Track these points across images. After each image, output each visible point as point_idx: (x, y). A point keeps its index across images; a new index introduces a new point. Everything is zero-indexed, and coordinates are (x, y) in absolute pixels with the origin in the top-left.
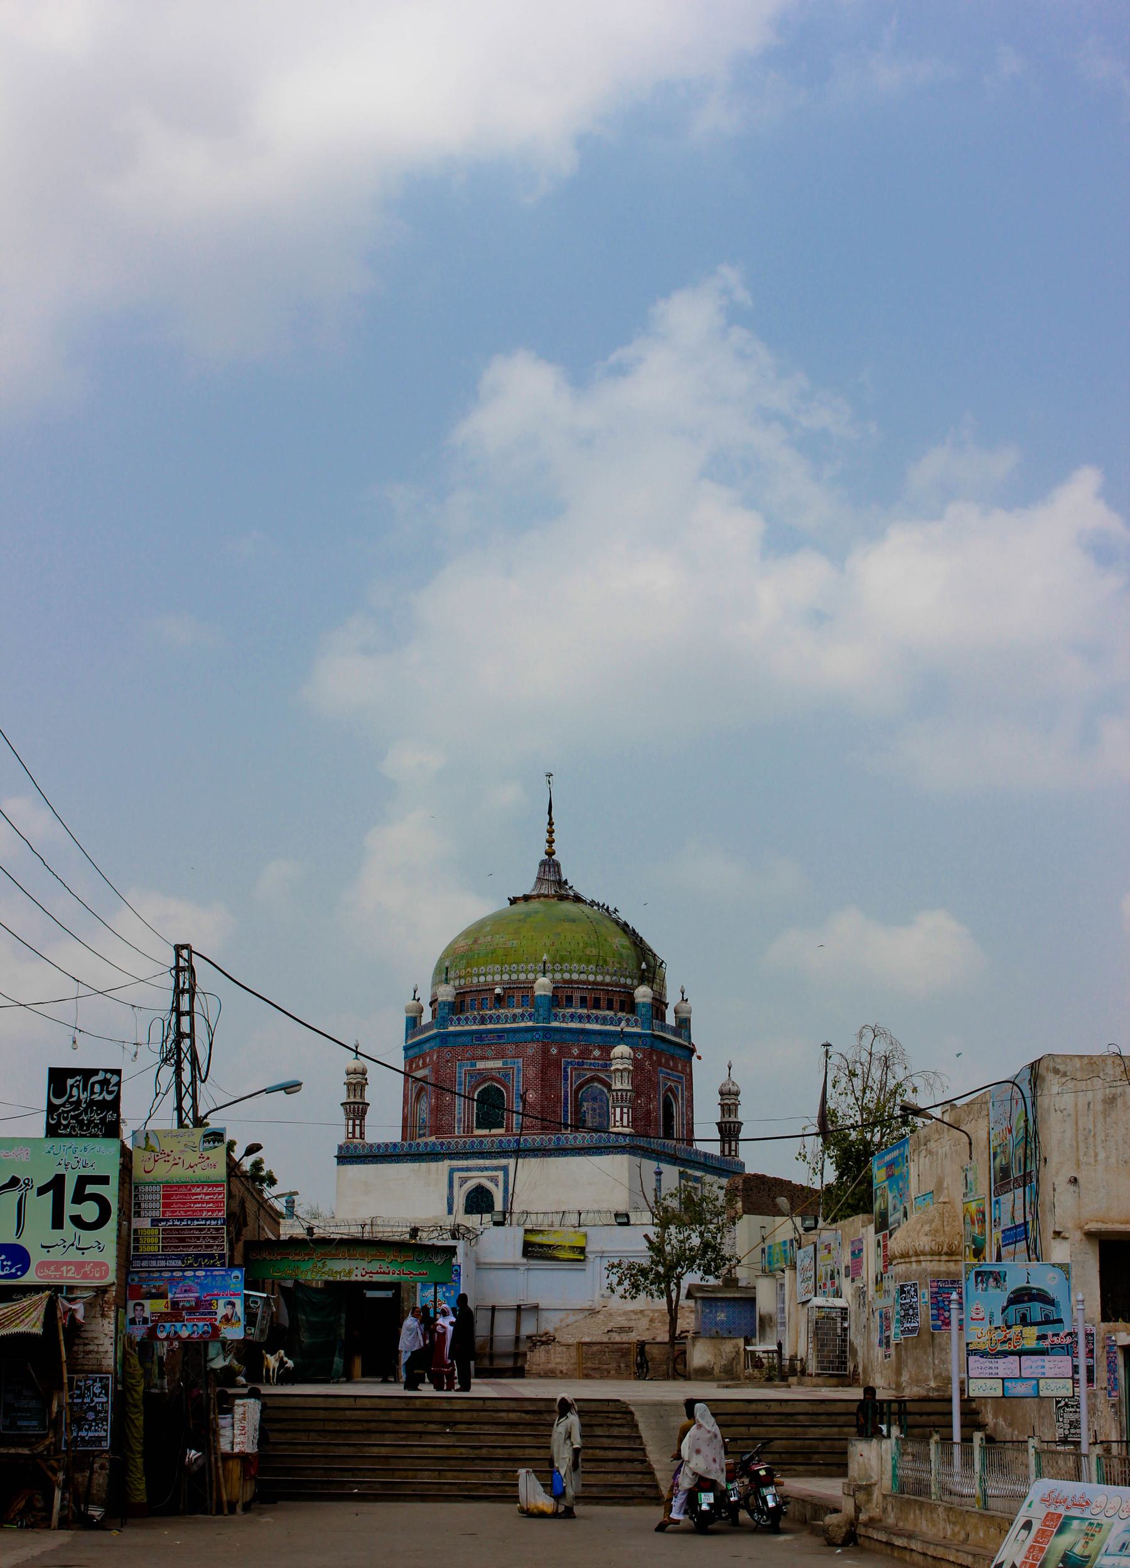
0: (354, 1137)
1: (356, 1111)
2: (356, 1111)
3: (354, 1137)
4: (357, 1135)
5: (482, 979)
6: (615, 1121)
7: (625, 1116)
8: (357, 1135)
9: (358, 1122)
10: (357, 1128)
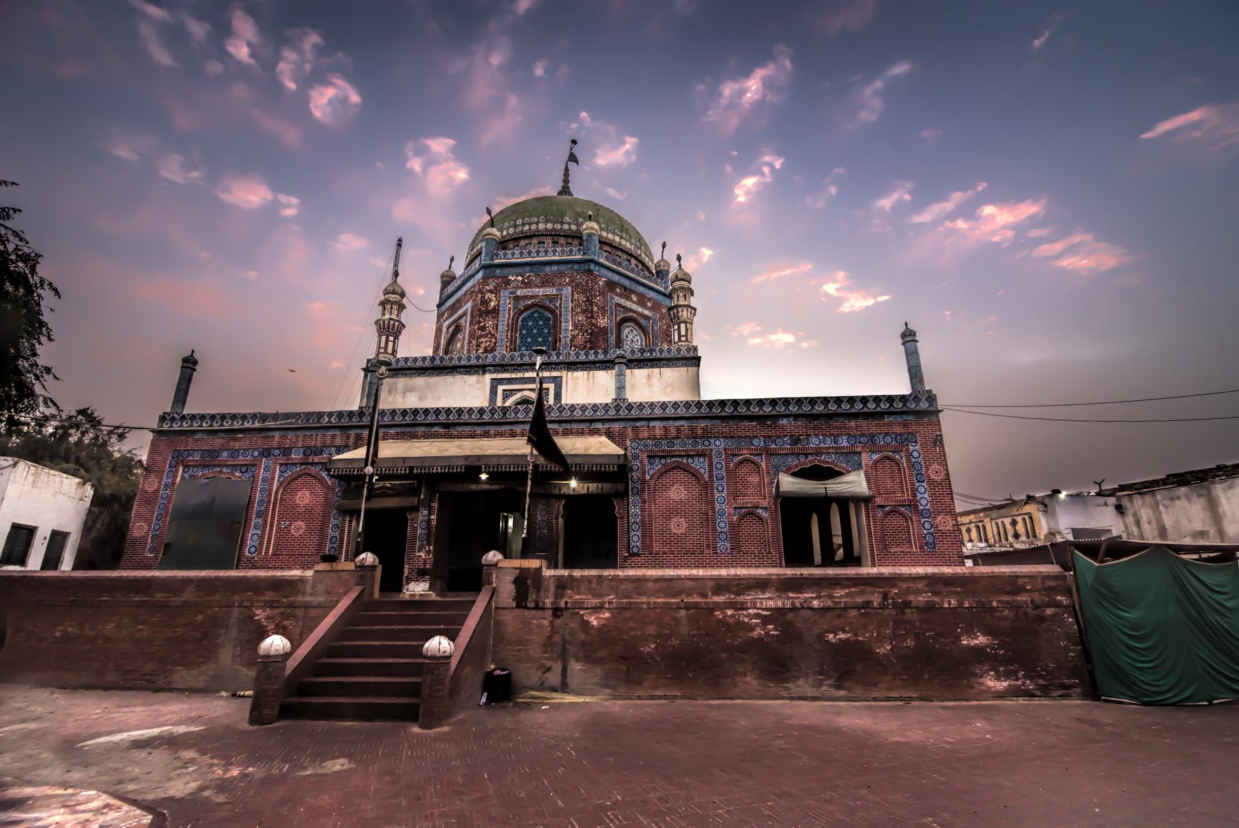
1: (390, 330)
2: (390, 330)
3: (386, 352)
4: (390, 350)
5: (527, 228)
6: (680, 336)
7: (683, 333)
8: (390, 350)
9: (391, 338)
10: (390, 344)
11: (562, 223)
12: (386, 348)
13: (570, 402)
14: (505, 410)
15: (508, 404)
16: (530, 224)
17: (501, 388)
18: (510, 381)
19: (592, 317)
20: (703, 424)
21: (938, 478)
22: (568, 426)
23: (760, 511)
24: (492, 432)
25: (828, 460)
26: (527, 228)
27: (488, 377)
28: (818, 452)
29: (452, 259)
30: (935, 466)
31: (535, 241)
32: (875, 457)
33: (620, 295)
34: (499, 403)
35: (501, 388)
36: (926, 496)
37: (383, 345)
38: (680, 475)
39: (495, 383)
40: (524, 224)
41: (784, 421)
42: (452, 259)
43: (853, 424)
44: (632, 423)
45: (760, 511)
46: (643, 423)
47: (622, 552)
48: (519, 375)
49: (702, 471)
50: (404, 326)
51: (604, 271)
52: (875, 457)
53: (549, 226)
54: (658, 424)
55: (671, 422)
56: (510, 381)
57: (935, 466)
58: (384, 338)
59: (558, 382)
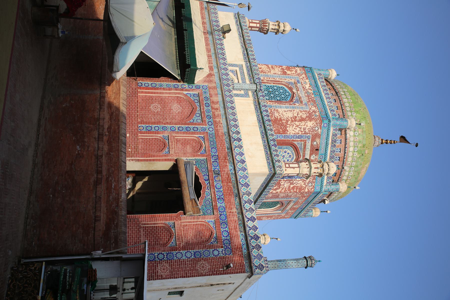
0: (250, 22)
5: (342, 93)
7: (291, 165)
8: (252, 25)
9: (258, 25)
10: (255, 25)
11: (351, 111)
12: (252, 23)
13: (236, 101)
14: (227, 75)
15: (231, 74)
16: (345, 94)
17: (238, 69)
18: (242, 73)
19: (292, 121)
20: (223, 121)
21: (198, 267)
22: (213, 57)
23: (167, 150)
24: (205, 25)
25: (206, 192)
26: (342, 93)
27: (244, 63)
28: (212, 186)
29: (319, 261)
30: (208, 266)
31: (336, 97)
32: (212, 225)
33: (312, 145)
34: (230, 68)
35: (238, 69)
36: (184, 258)
37: (253, 21)
38: (187, 111)
39: (241, 67)
40: (344, 92)
41: (230, 167)
42: (319, 261)
43: (234, 210)
44: (219, 86)
45: (167, 150)
46: (220, 92)
47: (122, 40)
48: (247, 77)
49: (192, 121)
50: (267, 33)
51: (325, 130)
52: (212, 225)
53: (347, 104)
54: (220, 98)
55: (222, 105)
56: (242, 73)
57: (208, 266)
58: (258, 22)
59: (246, 95)
